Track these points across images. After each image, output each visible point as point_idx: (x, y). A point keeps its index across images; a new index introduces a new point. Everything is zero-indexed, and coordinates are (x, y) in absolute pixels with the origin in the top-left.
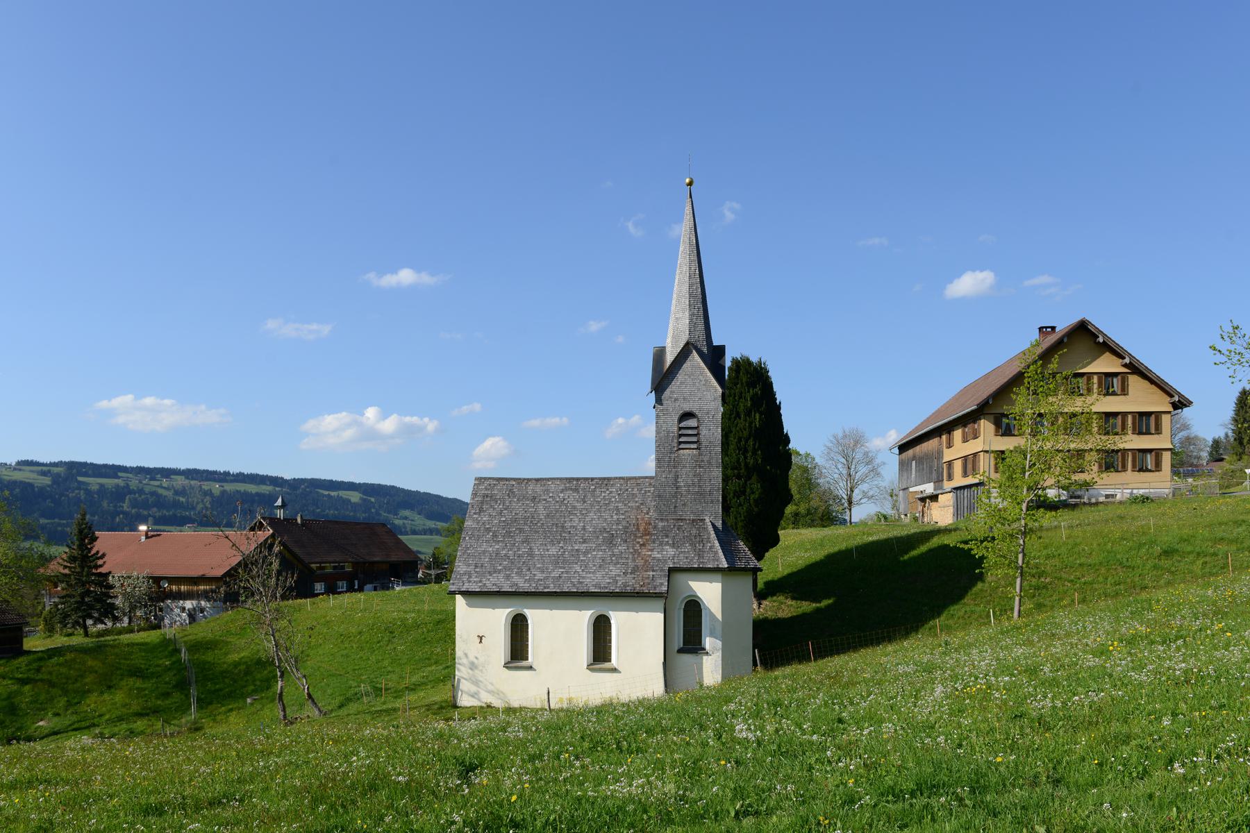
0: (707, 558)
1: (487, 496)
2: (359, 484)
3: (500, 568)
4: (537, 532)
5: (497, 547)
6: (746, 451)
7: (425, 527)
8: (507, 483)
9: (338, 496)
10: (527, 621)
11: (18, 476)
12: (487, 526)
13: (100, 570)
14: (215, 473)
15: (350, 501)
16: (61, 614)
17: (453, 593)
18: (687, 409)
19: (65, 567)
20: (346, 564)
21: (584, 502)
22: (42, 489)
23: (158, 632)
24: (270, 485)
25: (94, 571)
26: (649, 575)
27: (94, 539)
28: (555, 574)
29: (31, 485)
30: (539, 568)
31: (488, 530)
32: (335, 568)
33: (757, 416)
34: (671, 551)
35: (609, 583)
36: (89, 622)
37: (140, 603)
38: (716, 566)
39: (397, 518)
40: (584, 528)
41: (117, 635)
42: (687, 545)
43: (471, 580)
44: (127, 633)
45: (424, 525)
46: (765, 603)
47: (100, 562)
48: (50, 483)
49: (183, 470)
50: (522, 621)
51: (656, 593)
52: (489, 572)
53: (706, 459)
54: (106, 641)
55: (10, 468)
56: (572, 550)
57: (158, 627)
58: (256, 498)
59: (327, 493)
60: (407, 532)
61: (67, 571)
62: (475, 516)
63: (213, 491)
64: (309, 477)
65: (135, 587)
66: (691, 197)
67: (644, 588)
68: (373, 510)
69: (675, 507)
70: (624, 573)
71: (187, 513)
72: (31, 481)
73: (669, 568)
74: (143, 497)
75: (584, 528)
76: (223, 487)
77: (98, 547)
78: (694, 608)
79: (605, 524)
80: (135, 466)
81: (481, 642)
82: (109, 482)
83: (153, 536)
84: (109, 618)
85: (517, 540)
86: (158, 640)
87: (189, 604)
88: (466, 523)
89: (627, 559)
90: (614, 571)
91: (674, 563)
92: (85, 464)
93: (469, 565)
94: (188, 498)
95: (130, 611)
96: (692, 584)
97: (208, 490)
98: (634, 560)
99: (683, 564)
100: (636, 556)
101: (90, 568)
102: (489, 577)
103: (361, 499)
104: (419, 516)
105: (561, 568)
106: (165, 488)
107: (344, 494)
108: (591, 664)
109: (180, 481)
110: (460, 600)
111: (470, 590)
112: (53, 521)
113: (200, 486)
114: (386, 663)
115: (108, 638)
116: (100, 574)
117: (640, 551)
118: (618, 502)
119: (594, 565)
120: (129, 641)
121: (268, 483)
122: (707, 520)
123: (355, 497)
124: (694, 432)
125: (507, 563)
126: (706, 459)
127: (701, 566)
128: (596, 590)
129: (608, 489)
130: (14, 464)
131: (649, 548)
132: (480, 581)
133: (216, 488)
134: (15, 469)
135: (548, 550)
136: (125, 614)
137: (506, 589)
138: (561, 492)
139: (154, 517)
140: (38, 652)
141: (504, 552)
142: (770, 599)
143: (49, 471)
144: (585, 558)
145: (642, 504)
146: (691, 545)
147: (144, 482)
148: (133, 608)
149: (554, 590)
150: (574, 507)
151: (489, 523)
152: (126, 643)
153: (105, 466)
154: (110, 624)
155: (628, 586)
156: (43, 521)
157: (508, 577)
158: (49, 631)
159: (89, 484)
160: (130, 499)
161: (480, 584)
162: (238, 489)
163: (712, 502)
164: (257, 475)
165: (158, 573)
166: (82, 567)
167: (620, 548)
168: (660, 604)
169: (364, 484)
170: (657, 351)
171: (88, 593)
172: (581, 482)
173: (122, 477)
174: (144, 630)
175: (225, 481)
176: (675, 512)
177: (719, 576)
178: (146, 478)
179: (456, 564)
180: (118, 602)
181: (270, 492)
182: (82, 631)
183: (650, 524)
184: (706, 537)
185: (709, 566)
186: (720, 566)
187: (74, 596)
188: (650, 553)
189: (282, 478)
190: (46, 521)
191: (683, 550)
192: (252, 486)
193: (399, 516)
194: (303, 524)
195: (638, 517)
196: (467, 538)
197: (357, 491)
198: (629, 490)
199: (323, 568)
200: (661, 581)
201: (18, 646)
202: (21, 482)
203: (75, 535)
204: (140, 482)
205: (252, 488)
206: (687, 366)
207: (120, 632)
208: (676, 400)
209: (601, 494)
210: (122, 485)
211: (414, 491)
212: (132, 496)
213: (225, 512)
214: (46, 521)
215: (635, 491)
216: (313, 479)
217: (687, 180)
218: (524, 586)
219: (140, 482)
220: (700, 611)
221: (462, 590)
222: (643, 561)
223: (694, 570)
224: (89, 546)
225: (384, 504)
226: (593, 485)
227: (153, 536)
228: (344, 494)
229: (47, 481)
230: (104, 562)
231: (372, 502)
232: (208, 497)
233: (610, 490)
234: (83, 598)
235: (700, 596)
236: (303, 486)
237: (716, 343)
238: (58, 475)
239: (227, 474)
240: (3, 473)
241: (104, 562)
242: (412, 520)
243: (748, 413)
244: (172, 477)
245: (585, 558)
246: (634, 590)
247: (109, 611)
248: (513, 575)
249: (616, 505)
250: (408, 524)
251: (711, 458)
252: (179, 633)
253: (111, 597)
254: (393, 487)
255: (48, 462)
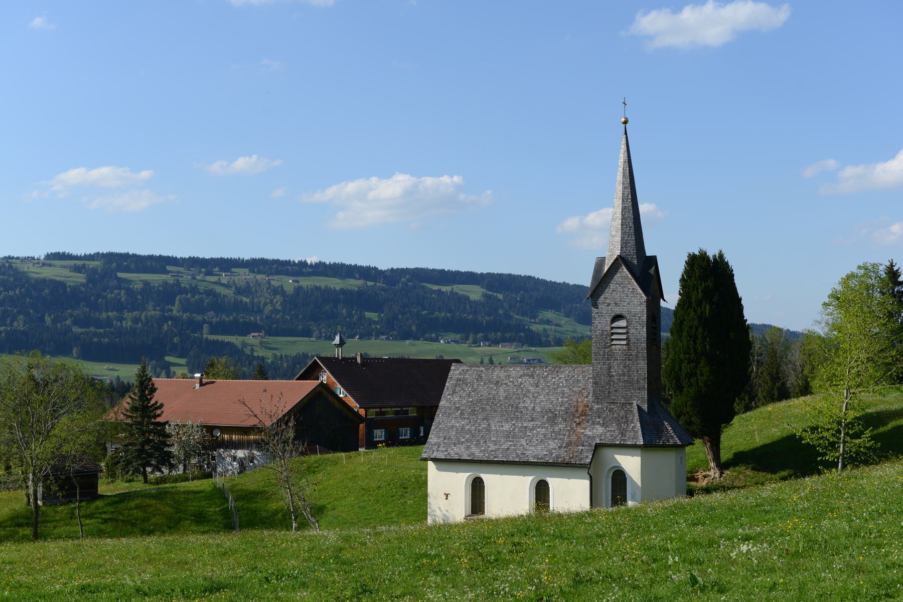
0: (629, 436)
1: (460, 380)
2: (482, 274)
3: (463, 440)
4: (495, 411)
5: (463, 423)
6: (696, 337)
7: (575, 335)
8: (478, 369)
9: (452, 292)
10: (484, 483)
11: (47, 273)
12: (457, 406)
13: (158, 420)
14: (287, 263)
15: (468, 298)
16: (124, 461)
17: (426, 460)
18: (618, 313)
19: (128, 417)
20: (411, 408)
21: (537, 386)
22: (75, 289)
23: (210, 481)
24: (359, 279)
25: (153, 420)
26: (579, 449)
27: (153, 390)
28: (505, 447)
29: (62, 284)
30: (494, 441)
31: (457, 409)
32: (397, 413)
33: (708, 307)
34: (600, 430)
35: (546, 455)
36: (149, 469)
37: (195, 451)
38: (634, 443)
39: (535, 323)
40: (534, 409)
41: (173, 482)
42: (614, 425)
43: (440, 449)
44: (182, 481)
45: (574, 332)
46: (727, 472)
47: (159, 412)
48: (84, 281)
49: (247, 261)
50: (480, 483)
51: (581, 464)
52: (454, 443)
53: (634, 353)
54: (164, 488)
55: (38, 263)
56: (522, 427)
57: (209, 476)
58: (341, 296)
59: (436, 288)
60: (549, 342)
61: (129, 421)
62: (449, 397)
63: (285, 288)
64: (412, 266)
65: (189, 436)
66: (626, 133)
67: (572, 460)
68: (501, 312)
69: (609, 392)
70: (559, 447)
71: (252, 318)
72: (62, 279)
73: (596, 443)
74: (197, 297)
75: (534, 409)
76: (297, 282)
77: (157, 397)
78: (619, 477)
79: (551, 406)
80: (187, 257)
81: (447, 498)
82: (155, 279)
83: (207, 383)
84: (166, 466)
85: (479, 417)
86: (210, 489)
87: (240, 454)
88: (441, 403)
89: (564, 435)
90: (552, 445)
91: (601, 440)
92: (126, 256)
93: (439, 437)
94: (253, 299)
95: (185, 460)
96: (617, 457)
97: (279, 287)
98: (569, 436)
99: (607, 441)
100: (571, 433)
101: (149, 417)
102: (453, 447)
103: (484, 295)
104: (567, 319)
105: (510, 441)
106: (223, 285)
107: (460, 289)
108: (469, 516)
109: (243, 276)
110: (431, 465)
111: (437, 457)
112: (87, 330)
113: (269, 282)
114: (394, 515)
115: (167, 485)
116: (159, 424)
117: (575, 429)
118: (565, 387)
119: (537, 440)
120: (185, 489)
121: (357, 276)
122: (635, 404)
123: (475, 293)
124: (624, 331)
125: (468, 436)
126: (634, 353)
127: (622, 443)
128: (534, 461)
129: (558, 376)
130: (42, 257)
131: (584, 426)
132: (446, 451)
133: (289, 283)
134: (44, 264)
135: (502, 426)
136: (180, 463)
137: (465, 457)
138: (520, 378)
139: (210, 324)
140: (111, 496)
141: (468, 427)
142: (731, 469)
143: (84, 266)
144: (531, 434)
145: (584, 389)
146: (617, 425)
147: (198, 278)
148: (188, 456)
149: (502, 459)
150: (528, 391)
151: (459, 403)
152: (183, 490)
153: (151, 258)
154: (166, 471)
155: (560, 458)
156: (76, 330)
157: (468, 448)
158: (112, 477)
159: (131, 281)
160: (180, 301)
161: (446, 453)
162: (318, 284)
163: (639, 389)
164: (343, 265)
165: (212, 422)
166: (143, 417)
167: (560, 426)
168: (585, 472)
169: (488, 274)
170: (598, 261)
171: (148, 441)
172: (537, 369)
173: (171, 272)
174: (198, 478)
175: (302, 274)
176: (609, 396)
177: (639, 451)
178: (200, 272)
179: (430, 436)
180: (174, 450)
181: (359, 287)
182: (141, 478)
183: (588, 406)
184: (631, 418)
185: (628, 443)
186: (638, 443)
187: (135, 444)
188: (583, 431)
189: (376, 269)
190: (80, 330)
191: (610, 429)
192: (337, 280)
193: (537, 320)
194: (363, 364)
195: (579, 400)
196: (440, 415)
197: (479, 284)
198: (575, 376)
199: (384, 413)
200: (587, 455)
201: (94, 490)
202: (51, 281)
203: (137, 387)
204: (194, 278)
205: (336, 284)
206: (617, 277)
207: (176, 480)
208: (609, 304)
209: (552, 379)
210: (171, 282)
211: (560, 284)
212: (184, 296)
213: (300, 316)
214: (80, 330)
215: (580, 378)
216: (417, 269)
217: (623, 120)
218: (478, 455)
219: (194, 278)
220: (625, 479)
221: (431, 457)
222: (576, 437)
223: (615, 446)
224: (149, 397)
225: (517, 301)
226: (546, 371)
227: (207, 383)
228: (460, 289)
229: (81, 278)
230: (162, 412)
231: (499, 300)
232: (278, 296)
233: (560, 376)
234: (143, 446)
235: (623, 466)
236: (403, 279)
237: (648, 254)
238: (94, 271)
239: (303, 264)
240: (31, 270)
241: (162, 412)
242: (557, 325)
243: (699, 304)
244: (233, 270)
245: (531, 434)
246: (564, 461)
247: (166, 459)
248: (472, 446)
249: (563, 389)
250: (551, 329)
251: (638, 352)
252: (228, 482)
253: (168, 446)
254: (529, 278)
255: (83, 255)
